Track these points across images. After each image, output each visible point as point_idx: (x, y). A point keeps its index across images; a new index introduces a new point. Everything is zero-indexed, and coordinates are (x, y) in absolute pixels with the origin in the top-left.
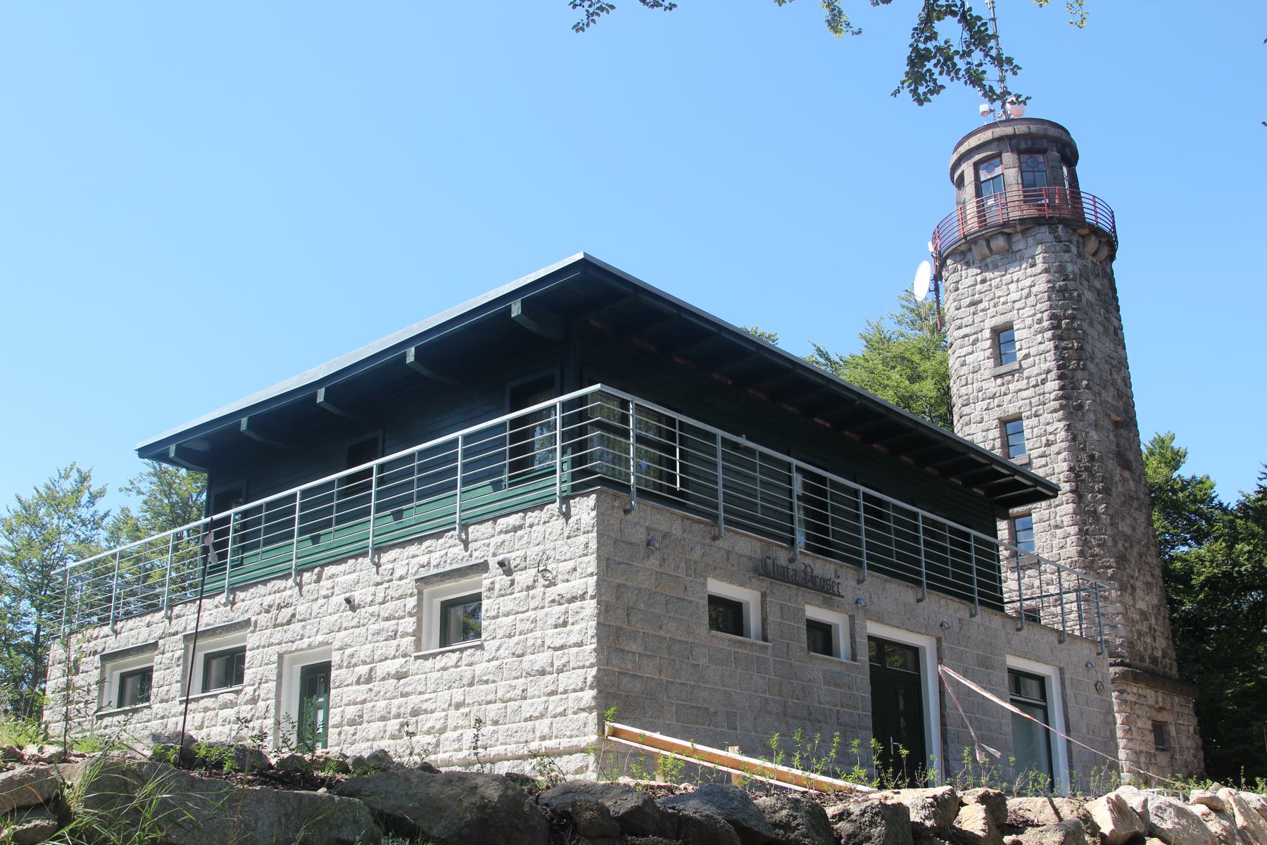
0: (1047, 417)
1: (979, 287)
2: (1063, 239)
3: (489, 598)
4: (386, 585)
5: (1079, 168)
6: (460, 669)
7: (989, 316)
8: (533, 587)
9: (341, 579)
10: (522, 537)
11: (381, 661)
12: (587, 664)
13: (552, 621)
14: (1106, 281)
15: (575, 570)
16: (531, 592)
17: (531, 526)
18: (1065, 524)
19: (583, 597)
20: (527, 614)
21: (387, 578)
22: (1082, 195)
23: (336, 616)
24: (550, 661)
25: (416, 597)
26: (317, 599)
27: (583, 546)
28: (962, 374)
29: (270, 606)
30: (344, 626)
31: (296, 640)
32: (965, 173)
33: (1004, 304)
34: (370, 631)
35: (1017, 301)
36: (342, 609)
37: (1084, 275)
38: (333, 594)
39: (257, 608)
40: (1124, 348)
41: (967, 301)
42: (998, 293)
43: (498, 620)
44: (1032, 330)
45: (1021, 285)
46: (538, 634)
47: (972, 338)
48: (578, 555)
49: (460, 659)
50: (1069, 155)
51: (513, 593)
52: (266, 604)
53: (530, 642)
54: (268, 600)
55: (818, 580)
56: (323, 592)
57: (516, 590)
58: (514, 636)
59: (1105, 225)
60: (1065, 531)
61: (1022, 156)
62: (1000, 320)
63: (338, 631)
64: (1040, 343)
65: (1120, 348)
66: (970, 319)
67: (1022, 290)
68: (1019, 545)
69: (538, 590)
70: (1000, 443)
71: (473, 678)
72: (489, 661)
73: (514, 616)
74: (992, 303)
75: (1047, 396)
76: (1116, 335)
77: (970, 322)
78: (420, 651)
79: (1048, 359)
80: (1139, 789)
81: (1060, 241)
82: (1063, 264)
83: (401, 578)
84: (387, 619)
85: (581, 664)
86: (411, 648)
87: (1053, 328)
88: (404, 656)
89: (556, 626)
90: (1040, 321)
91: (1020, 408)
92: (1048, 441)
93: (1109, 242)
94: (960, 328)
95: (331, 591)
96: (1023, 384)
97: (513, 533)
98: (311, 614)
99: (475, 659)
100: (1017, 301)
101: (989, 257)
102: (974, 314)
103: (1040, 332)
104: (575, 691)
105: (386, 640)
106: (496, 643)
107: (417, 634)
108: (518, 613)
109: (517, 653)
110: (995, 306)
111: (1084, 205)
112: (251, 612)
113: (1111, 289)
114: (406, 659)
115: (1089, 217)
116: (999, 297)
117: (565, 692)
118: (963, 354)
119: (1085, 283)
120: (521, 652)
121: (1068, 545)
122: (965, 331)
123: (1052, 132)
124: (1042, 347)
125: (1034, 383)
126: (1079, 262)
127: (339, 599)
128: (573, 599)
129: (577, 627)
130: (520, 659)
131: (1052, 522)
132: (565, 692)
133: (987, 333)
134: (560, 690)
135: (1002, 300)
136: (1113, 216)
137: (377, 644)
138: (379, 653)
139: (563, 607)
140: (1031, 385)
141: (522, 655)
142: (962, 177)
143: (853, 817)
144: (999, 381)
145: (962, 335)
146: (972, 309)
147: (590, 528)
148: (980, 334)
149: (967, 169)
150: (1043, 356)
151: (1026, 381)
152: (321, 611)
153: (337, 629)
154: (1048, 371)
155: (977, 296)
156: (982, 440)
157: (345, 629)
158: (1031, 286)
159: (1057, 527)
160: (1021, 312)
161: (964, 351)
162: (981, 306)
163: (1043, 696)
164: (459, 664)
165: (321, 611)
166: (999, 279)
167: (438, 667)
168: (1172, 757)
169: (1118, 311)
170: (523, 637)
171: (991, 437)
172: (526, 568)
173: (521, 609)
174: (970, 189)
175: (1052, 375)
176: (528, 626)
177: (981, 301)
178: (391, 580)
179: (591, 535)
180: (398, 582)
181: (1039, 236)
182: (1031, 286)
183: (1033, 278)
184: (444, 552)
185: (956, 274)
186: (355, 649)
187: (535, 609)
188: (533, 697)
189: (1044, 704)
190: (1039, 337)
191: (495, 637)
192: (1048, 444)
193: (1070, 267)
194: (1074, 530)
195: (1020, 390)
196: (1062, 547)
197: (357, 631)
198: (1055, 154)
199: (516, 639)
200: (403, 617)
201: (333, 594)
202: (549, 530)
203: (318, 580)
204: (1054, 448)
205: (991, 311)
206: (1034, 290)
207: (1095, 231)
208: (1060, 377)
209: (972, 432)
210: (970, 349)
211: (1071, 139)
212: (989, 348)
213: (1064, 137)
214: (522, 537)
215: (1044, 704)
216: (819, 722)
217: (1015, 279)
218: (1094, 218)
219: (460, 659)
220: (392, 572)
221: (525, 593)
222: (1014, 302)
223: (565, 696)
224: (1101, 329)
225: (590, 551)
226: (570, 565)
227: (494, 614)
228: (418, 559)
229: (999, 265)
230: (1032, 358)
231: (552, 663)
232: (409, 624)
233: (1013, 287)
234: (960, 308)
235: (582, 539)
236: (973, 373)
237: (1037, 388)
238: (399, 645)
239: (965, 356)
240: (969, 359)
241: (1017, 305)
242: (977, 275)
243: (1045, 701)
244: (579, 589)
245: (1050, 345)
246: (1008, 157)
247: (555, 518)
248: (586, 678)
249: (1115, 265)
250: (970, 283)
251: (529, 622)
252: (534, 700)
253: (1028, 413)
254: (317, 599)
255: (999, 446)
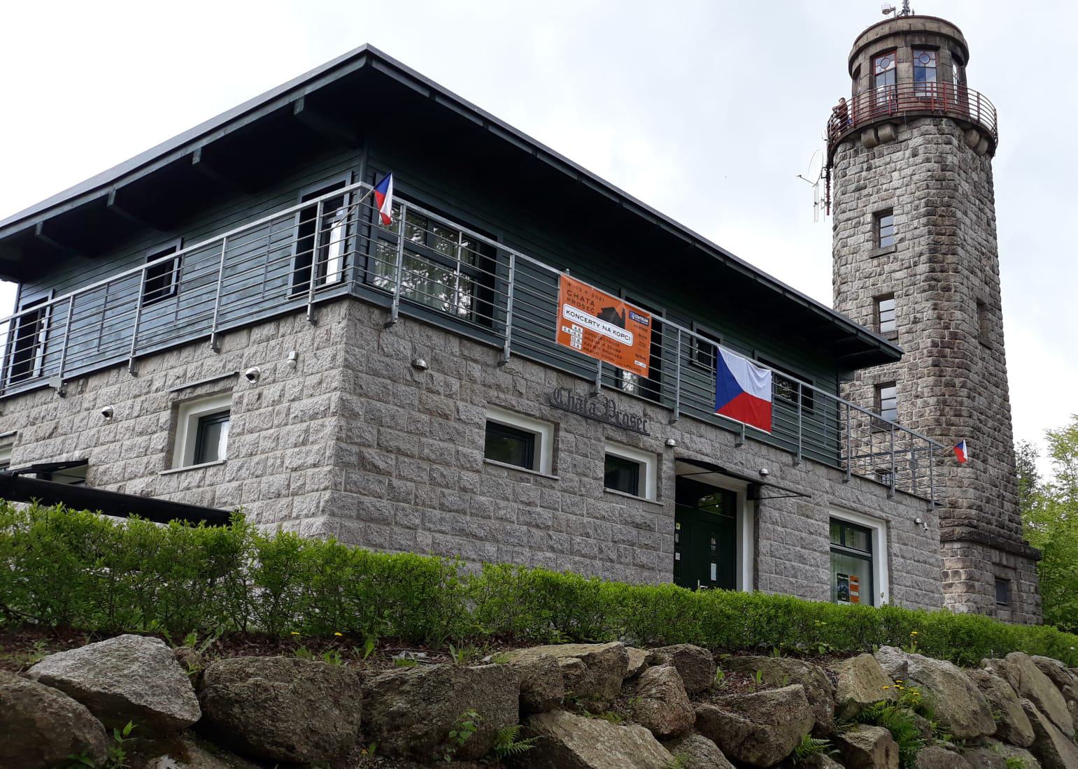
0: (919, 297)
1: (864, 174)
2: (946, 131)
3: (236, 413)
4: (143, 398)
5: (969, 69)
6: (201, 489)
7: (872, 201)
8: (280, 402)
9: (104, 391)
10: (274, 348)
11: (130, 479)
12: (322, 487)
13: (292, 440)
14: (983, 175)
15: (320, 383)
16: (277, 408)
17: (283, 336)
18: (926, 395)
19: (325, 414)
20: (271, 431)
21: (144, 391)
22: (969, 91)
23: (95, 430)
24: (286, 483)
25: (169, 411)
26: (79, 412)
27: (329, 358)
28: (843, 254)
29: (36, 419)
30: (101, 441)
31: (55, 455)
32: (862, 67)
33: (886, 190)
34: (124, 447)
35: (898, 188)
36: (100, 424)
37: (963, 168)
38: (94, 406)
39: (23, 421)
40: (995, 238)
41: (853, 187)
42: (883, 180)
43: (243, 438)
44: (910, 216)
45: (904, 173)
46: (278, 453)
47: (855, 221)
48: (324, 368)
49: (203, 478)
50: (960, 54)
51: (260, 408)
52: (32, 415)
53: (270, 462)
54: (34, 413)
55: (621, 417)
56: (85, 405)
57: (263, 405)
58: (256, 455)
59: (987, 121)
60: (925, 401)
61: (915, 52)
62: (881, 206)
63: (95, 447)
64: (915, 228)
65: (991, 238)
66: (854, 204)
67: (904, 178)
68: (882, 412)
69: (284, 405)
70: (872, 319)
71: (213, 499)
72: (230, 481)
73: (257, 434)
74: (875, 189)
75: (918, 277)
76: (989, 226)
77: (855, 207)
78: (170, 469)
79: (923, 243)
80: (871, 652)
81: (943, 134)
82: (944, 155)
83: (157, 390)
84: (141, 434)
85: (316, 487)
86: (160, 465)
87: (928, 214)
88: (152, 473)
89: (296, 446)
90: (917, 208)
91: (892, 287)
92: (915, 318)
93: (987, 140)
94: (844, 212)
95: (92, 404)
96: (896, 266)
97: (266, 344)
98: (72, 429)
99: (219, 478)
100: (898, 188)
101: (876, 146)
102: (858, 199)
103: (917, 218)
104: (307, 516)
105: (137, 457)
106: (238, 463)
107: (169, 450)
108: (261, 430)
109: (256, 473)
110: (877, 193)
111: (969, 96)
112: (18, 425)
113: (988, 183)
114: (153, 478)
115: (973, 113)
116: (882, 185)
117: (297, 517)
118: (845, 236)
119: (963, 175)
120: (260, 472)
121: (927, 414)
122: (851, 214)
123: (946, 30)
124: (917, 232)
125: (907, 265)
126: (959, 154)
127: (97, 413)
128: (314, 417)
129: (316, 447)
130: (258, 479)
131: (914, 393)
132: (297, 517)
133: (869, 218)
134: (294, 515)
135: (884, 186)
136: (995, 114)
137: (129, 461)
138: (129, 471)
139: (305, 425)
140: (904, 266)
141: (261, 476)
142: (858, 69)
143: (406, 687)
144: (875, 262)
145: (845, 219)
146: (857, 194)
147: (338, 339)
148: (862, 218)
149: (863, 60)
150: (917, 241)
151: (899, 263)
152: (82, 425)
153: (93, 444)
154: (921, 254)
155: (862, 182)
156: (856, 315)
157: (102, 444)
158: (912, 175)
159: (917, 397)
160: (901, 199)
161: (846, 234)
162: (865, 192)
163: (869, 548)
164: (202, 484)
165: (82, 425)
166: (883, 167)
167: (182, 487)
168: (1013, 612)
169: (993, 203)
170: (263, 456)
171: (864, 313)
172: (274, 381)
173: (265, 427)
174: (864, 82)
175: (924, 258)
176: (269, 444)
177: (865, 188)
178: (148, 392)
179: (339, 347)
180: (155, 395)
181: (924, 128)
182: (912, 175)
183: (914, 167)
184: (200, 363)
185: (845, 161)
186: (108, 466)
187: (278, 426)
188: (267, 522)
189: (869, 555)
190: (915, 223)
191: (238, 455)
192: (916, 321)
193: (950, 158)
194: (932, 401)
195: (895, 271)
196: (921, 416)
197: (112, 446)
198: (945, 52)
199: (256, 459)
200: (154, 432)
201: (94, 406)
202: (300, 341)
203: (82, 392)
204: (920, 326)
205: (873, 199)
206: (915, 178)
207: (977, 126)
208: (931, 260)
209: (848, 308)
210: (852, 231)
211: (963, 39)
212: (869, 231)
213: (956, 36)
214: (274, 348)
215: (869, 555)
216: (612, 561)
217: (898, 168)
218: (976, 113)
219: (203, 478)
220: (151, 382)
221: (271, 408)
222: (896, 189)
223: (298, 521)
224: (974, 218)
225: (337, 363)
226: (317, 378)
227: (239, 430)
228: (176, 370)
229: (885, 153)
230: (907, 242)
231: (289, 485)
232: (160, 439)
233: (895, 175)
234: (845, 194)
235: (329, 352)
236: (853, 254)
237: (909, 270)
238: (148, 462)
239: (847, 238)
240: (851, 241)
241: (898, 192)
242: (864, 162)
243: (871, 552)
244: (321, 405)
245: (924, 230)
246: (903, 51)
247: (307, 327)
248: (319, 502)
249: (994, 161)
250: (858, 170)
251: (271, 440)
252: (268, 525)
253: (900, 292)
254: (79, 412)
255: (871, 322)
